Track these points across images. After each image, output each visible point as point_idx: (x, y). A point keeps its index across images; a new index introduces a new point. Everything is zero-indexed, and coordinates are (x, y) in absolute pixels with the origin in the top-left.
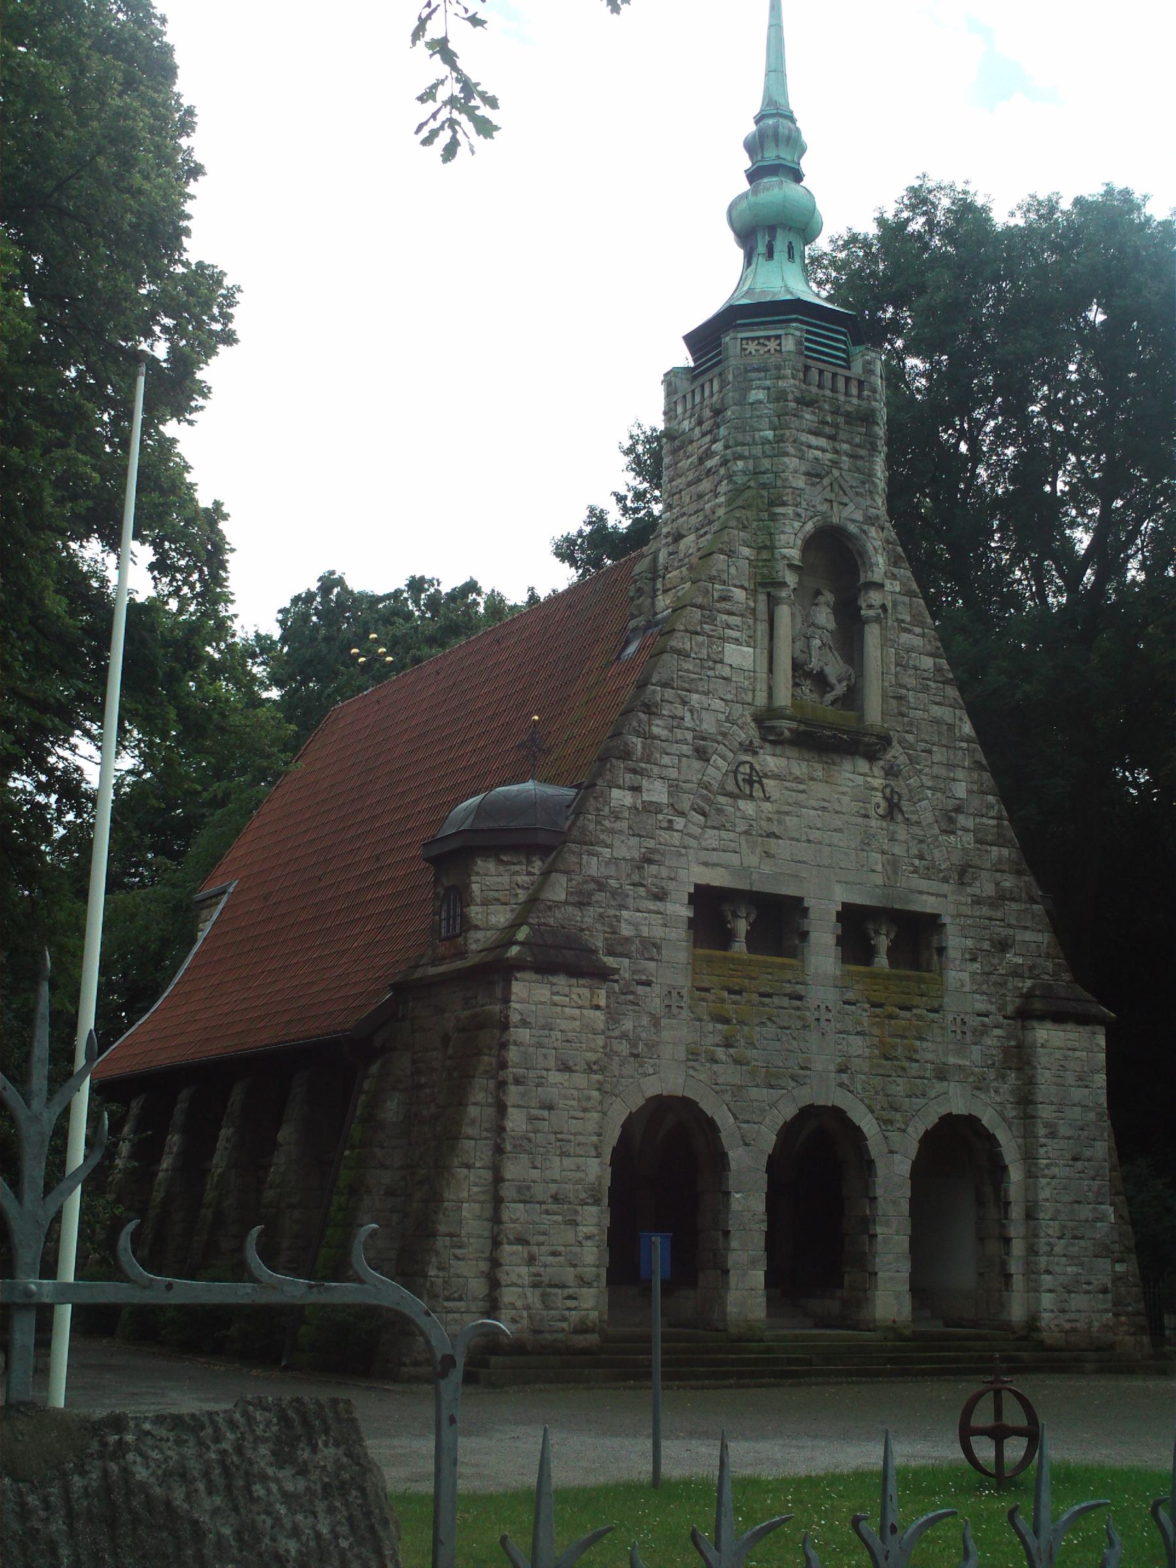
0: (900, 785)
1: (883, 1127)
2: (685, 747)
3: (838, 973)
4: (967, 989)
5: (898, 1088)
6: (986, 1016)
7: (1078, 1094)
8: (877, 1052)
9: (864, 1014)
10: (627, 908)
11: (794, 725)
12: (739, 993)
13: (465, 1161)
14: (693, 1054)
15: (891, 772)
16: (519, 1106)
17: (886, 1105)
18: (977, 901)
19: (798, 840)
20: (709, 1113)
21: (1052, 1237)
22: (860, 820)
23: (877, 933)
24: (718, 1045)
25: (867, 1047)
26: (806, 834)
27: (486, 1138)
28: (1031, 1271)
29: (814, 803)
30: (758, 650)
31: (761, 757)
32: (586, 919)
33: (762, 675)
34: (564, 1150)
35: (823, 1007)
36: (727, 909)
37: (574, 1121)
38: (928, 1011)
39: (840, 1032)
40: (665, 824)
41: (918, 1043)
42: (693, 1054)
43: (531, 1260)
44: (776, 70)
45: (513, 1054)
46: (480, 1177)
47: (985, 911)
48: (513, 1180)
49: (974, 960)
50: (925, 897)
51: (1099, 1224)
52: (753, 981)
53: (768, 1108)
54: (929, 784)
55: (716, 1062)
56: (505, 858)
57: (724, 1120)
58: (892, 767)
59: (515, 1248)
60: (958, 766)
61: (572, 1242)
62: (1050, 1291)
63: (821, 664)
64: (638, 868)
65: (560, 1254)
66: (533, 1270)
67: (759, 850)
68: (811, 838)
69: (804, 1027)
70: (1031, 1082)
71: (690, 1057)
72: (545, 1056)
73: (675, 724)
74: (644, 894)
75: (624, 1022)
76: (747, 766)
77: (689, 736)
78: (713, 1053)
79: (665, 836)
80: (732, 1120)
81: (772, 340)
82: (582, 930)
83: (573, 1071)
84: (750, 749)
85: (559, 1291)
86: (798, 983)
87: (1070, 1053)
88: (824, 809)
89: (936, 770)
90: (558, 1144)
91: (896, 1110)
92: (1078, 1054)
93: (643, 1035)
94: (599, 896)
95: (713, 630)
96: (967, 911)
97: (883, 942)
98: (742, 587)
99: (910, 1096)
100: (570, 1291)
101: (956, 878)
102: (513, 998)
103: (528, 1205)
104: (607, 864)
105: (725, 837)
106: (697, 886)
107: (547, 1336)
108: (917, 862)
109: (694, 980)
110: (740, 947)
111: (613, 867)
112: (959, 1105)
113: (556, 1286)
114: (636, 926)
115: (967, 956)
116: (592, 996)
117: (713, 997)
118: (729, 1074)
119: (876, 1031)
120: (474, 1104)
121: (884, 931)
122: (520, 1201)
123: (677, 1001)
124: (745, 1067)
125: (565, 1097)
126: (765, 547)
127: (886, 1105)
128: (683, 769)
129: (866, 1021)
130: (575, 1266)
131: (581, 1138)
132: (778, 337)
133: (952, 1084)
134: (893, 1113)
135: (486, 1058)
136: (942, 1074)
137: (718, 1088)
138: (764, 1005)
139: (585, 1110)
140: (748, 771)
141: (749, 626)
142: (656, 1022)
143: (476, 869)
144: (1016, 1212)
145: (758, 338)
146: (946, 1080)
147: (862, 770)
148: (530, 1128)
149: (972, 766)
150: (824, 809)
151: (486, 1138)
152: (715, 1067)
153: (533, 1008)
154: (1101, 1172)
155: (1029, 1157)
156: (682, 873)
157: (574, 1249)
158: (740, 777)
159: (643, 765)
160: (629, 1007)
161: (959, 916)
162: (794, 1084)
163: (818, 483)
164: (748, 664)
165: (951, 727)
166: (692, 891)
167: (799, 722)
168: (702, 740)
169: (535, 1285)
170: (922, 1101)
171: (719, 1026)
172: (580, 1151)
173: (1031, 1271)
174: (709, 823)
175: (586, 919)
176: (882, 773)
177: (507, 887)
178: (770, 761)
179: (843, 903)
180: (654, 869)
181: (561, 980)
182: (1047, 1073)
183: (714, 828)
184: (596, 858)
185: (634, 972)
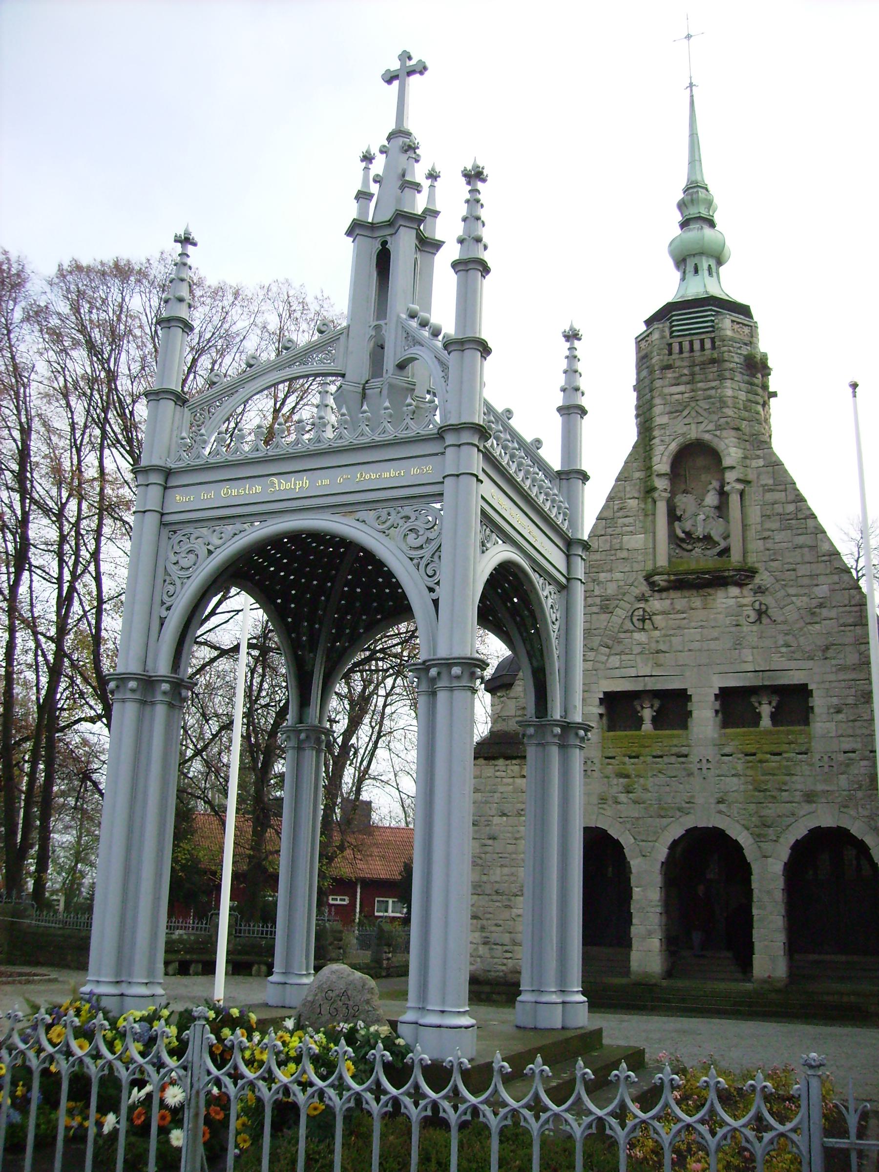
0: (768, 600)
5: (770, 811)
6: (854, 752)
8: (751, 787)
9: (740, 761)
11: (665, 577)
12: (637, 757)
14: (603, 800)
18: (842, 668)
20: (615, 837)
22: (734, 629)
23: (760, 704)
25: (743, 784)
29: (693, 624)
31: (650, 603)
35: (704, 761)
41: (787, 778)
42: (602, 799)
44: (694, 160)
49: (839, 711)
53: (660, 831)
55: (620, 803)
61: (508, 918)
63: (707, 530)
66: (484, 934)
72: (490, 808)
76: (641, 610)
77: (598, 600)
78: (616, 798)
80: (633, 840)
84: (643, 598)
88: (702, 627)
96: (833, 677)
98: (634, 498)
106: (605, 693)
107: (492, 973)
108: (784, 650)
109: (603, 752)
112: (827, 819)
113: (498, 944)
115: (832, 710)
124: (642, 805)
129: (740, 767)
130: (510, 933)
133: (820, 806)
136: (810, 797)
140: (641, 613)
146: (815, 802)
150: (702, 627)
152: (619, 806)
158: (635, 619)
161: (823, 682)
162: (681, 814)
167: (669, 574)
169: (485, 943)
171: (621, 780)
174: (613, 652)
176: (752, 594)
178: (656, 604)
181: (501, 762)
183: (616, 654)
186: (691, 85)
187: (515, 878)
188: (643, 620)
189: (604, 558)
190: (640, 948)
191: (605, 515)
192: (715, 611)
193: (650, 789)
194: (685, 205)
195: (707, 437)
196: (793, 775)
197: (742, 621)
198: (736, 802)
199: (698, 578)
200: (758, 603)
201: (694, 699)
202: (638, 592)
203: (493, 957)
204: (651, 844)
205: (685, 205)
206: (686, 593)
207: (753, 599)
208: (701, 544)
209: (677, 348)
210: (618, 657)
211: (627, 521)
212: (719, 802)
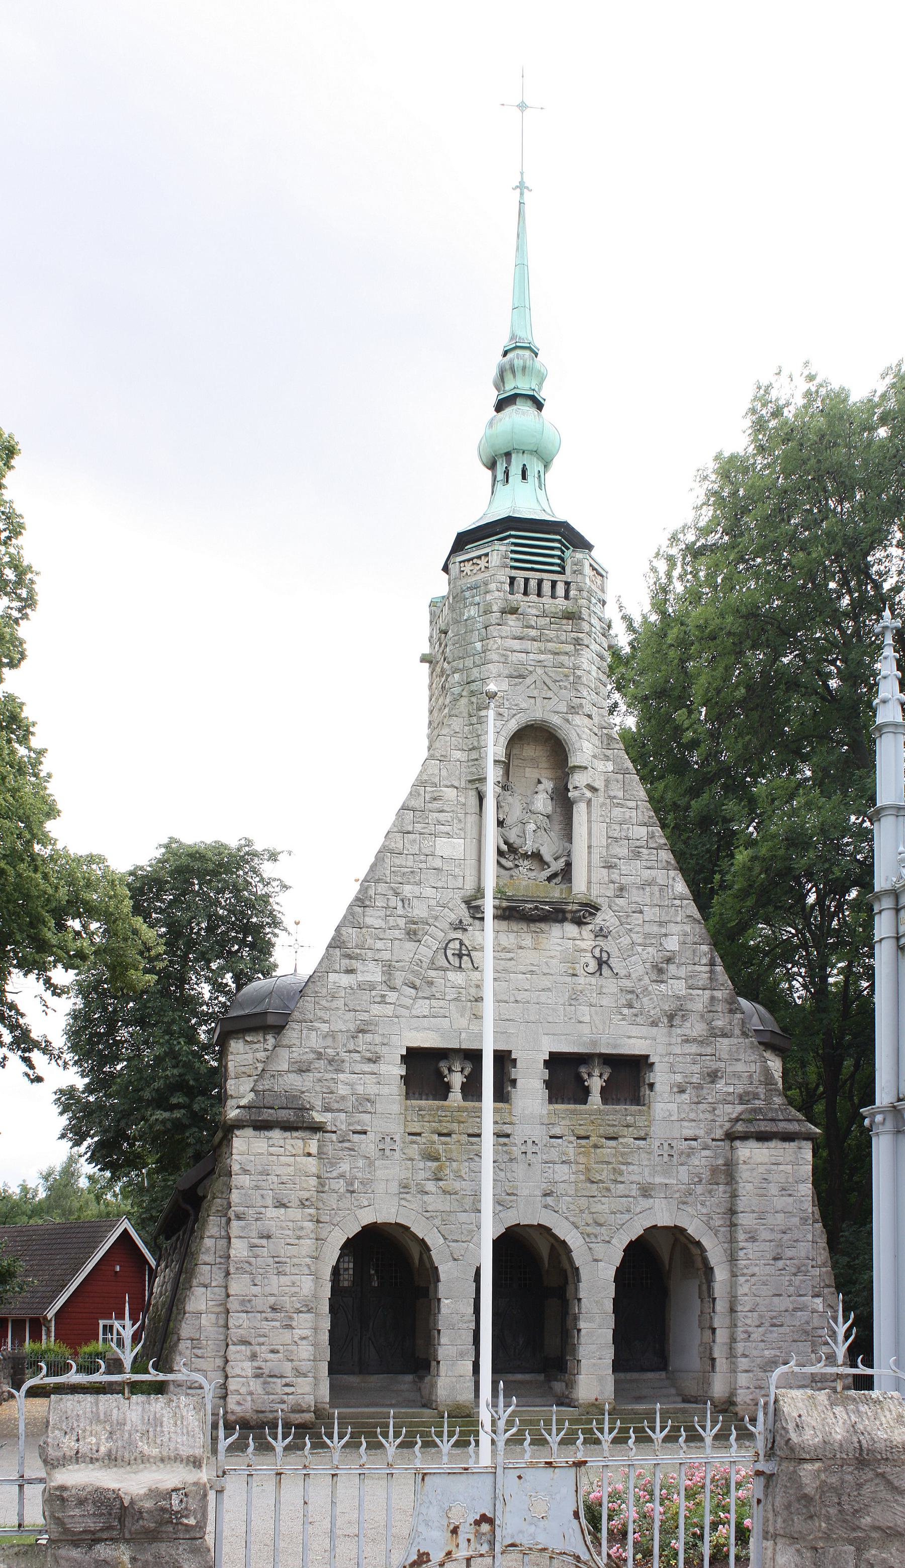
0: (609, 945)
1: (588, 1240)
2: (397, 932)
3: (545, 1112)
4: (674, 1118)
5: (603, 1207)
6: (695, 1140)
7: (781, 1202)
8: (582, 1177)
10: (343, 1072)
12: (448, 1135)
13: (202, 1282)
14: (405, 1187)
15: (601, 934)
16: (241, 1237)
17: (590, 1221)
19: (506, 1002)
21: (750, 1326)
22: (569, 979)
23: (590, 1075)
24: (429, 1180)
25: (573, 1173)
26: (514, 995)
27: (220, 1263)
28: (732, 1355)
29: (522, 968)
30: (468, 840)
31: (469, 933)
32: (306, 1083)
33: (472, 862)
34: (280, 1270)
35: (530, 1142)
36: (443, 1066)
37: (289, 1247)
38: (635, 1139)
39: (547, 1163)
40: (378, 999)
42: (404, 1187)
43: (254, 1356)
45: (235, 1196)
46: (215, 1294)
47: (694, 1049)
48: (236, 1295)
49: (682, 1091)
50: (633, 1041)
51: (799, 1313)
52: (462, 1125)
54: (640, 941)
55: (427, 1193)
56: (248, 1039)
57: (434, 1241)
58: (601, 929)
59: (239, 1348)
60: (670, 921)
61: (290, 1342)
62: (746, 1371)
63: (537, 845)
64: (353, 1037)
65: (278, 1352)
66: (255, 1364)
67: (468, 1014)
68: (518, 999)
69: (511, 1160)
70: (734, 1196)
71: (402, 1190)
72: (262, 1196)
73: (388, 913)
74: (359, 1059)
75: (341, 1165)
76: (457, 942)
77: (402, 922)
78: (423, 1186)
79: (376, 1009)
80: (442, 1241)
81: (483, 558)
82: (303, 1092)
83: (288, 1207)
85: (278, 1380)
86: (505, 1123)
87: (775, 1167)
88: (532, 972)
89: (648, 928)
90: (276, 1265)
91: (601, 1225)
92: (781, 1167)
93: (359, 1175)
94: (321, 1064)
95: (425, 828)
97: (596, 1084)
99: (615, 1213)
100: (287, 1380)
101: (666, 1021)
102: (234, 1151)
103: (250, 1314)
104: (325, 1037)
105: (435, 1005)
106: (408, 1049)
108: (625, 1011)
110: (595, 1098)
111: (330, 1039)
114: (351, 1085)
115: (675, 1089)
116: (305, 1146)
117: (424, 1140)
118: (436, 1202)
119: (582, 1159)
120: (209, 1237)
121: (597, 1072)
122: (243, 1311)
123: (390, 1145)
124: (453, 1196)
125: (282, 1228)
126: (474, 748)
127: (590, 1221)
128: (395, 951)
129: (571, 1151)
130: (292, 1360)
131: (295, 1260)
132: (487, 555)
134: (598, 1228)
135: (219, 1200)
136: (646, 1191)
137: (428, 1215)
138: (472, 1144)
139: (299, 1238)
140: (458, 946)
141: (460, 821)
142: (371, 1164)
143: (231, 1049)
144: (721, 1306)
145: (472, 559)
146: (652, 1197)
147: (570, 936)
148: (250, 1254)
149: (685, 920)
150: (532, 972)
151: (220, 1263)
152: (426, 1198)
153: (252, 1158)
154: (803, 1268)
155: (732, 1259)
156: (394, 1039)
157: (290, 1347)
158: (449, 953)
159: (358, 951)
160: (345, 1153)
163: (520, 683)
164: (458, 853)
165: (663, 888)
166: (404, 1053)
168: (414, 924)
169: (257, 1376)
170: (627, 1217)
171: (429, 1164)
172: (294, 1271)
173: (732, 1355)
174: (420, 994)
175: (306, 1083)
176: (592, 936)
177: (251, 1062)
179: (408, 1049)
180: (368, 1037)
182: (749, 1187)
184: (314, 1032)
185: (349, 1124)
186: (522, 187)
187: (297, 1289)
188: (460, 956)
189: (410, 864)
190: (450, 1373)
191: (413, 803)
192: (548, 954)
193: (466, 1177)
194: (513, 372)
195: (556, 720)
196: (629, 1164)
197: (579, 971)
198: (566, 1195)
199: (536, 908)
200: (598, 949)
201: (519, 1064)
202: (453, 916)
203: (268, 1393)
204: (465, 1245)
205: (513, 372)
206: (515, 926)
207: (594, 944)
208: (526, 862)
209: (522, 586)
210: (427, 1001)
211: (442, 817)
212: (545, 1195)
